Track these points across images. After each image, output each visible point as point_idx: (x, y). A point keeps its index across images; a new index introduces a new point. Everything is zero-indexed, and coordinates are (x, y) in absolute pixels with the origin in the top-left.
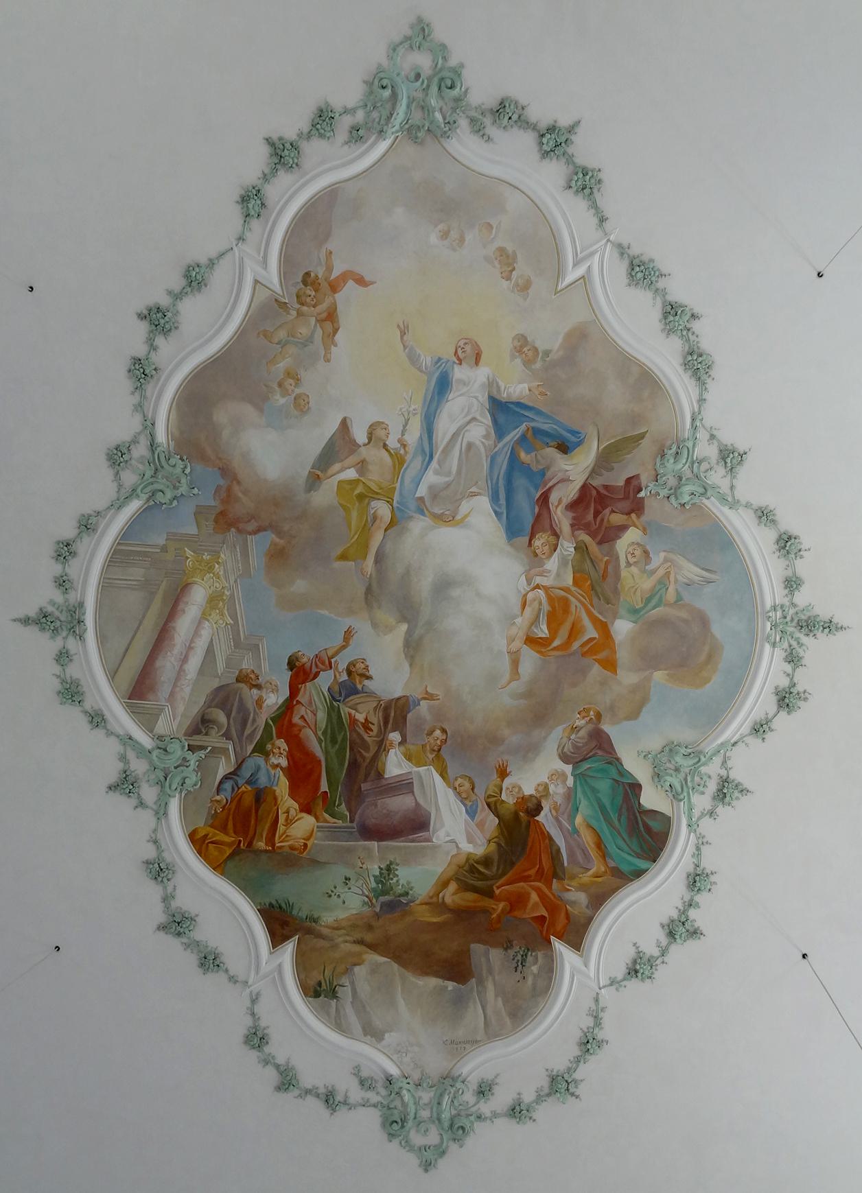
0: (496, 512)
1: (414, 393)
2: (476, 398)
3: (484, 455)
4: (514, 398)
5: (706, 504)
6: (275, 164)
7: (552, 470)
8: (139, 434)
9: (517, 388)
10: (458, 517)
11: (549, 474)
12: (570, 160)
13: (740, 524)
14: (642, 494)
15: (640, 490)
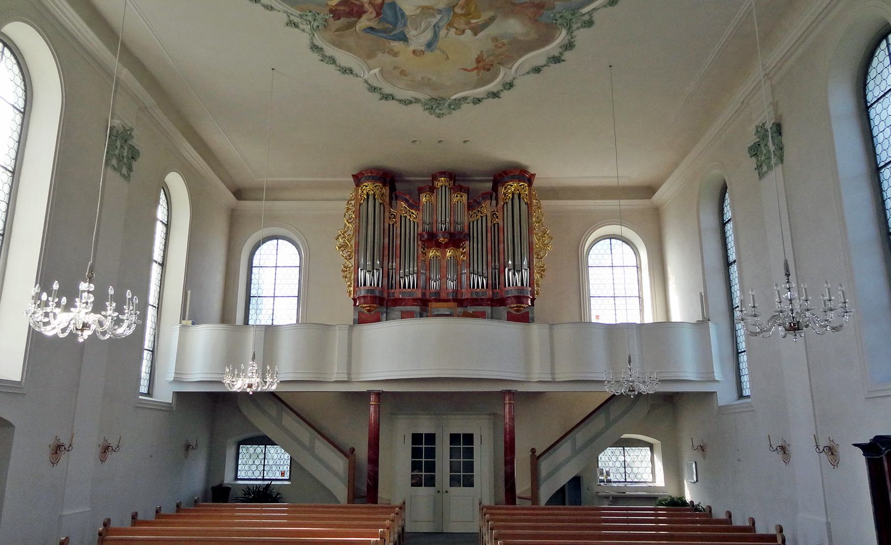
0: (402, 10)
1: (441, 43)
2: (414, 42)
3: (409, 26)
4: (396, 42)
5: (562, 34)
6: (31, 316)
7: (376, 22)
8: (575, 30)
9: (397, 45)
10: (420, 9)
11: (378, 21)
12: (561, 54)
13: (562, 36)
14: (331, 15)
15: (333, 17)
